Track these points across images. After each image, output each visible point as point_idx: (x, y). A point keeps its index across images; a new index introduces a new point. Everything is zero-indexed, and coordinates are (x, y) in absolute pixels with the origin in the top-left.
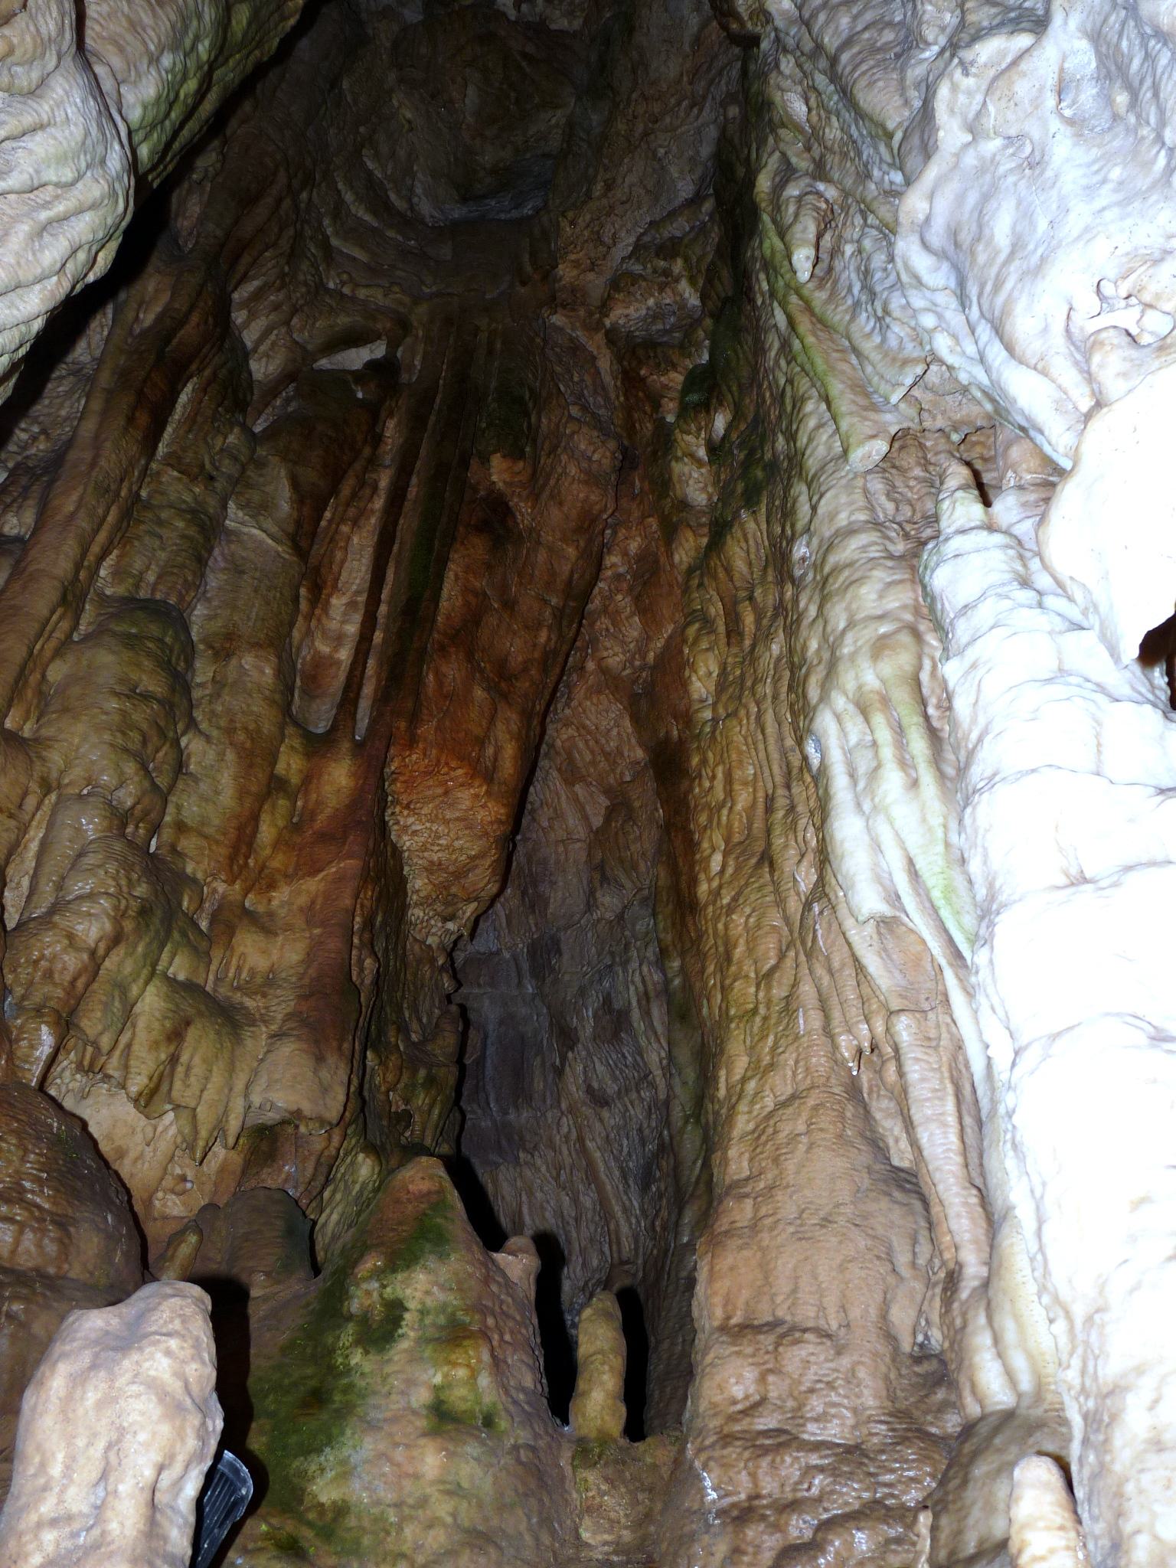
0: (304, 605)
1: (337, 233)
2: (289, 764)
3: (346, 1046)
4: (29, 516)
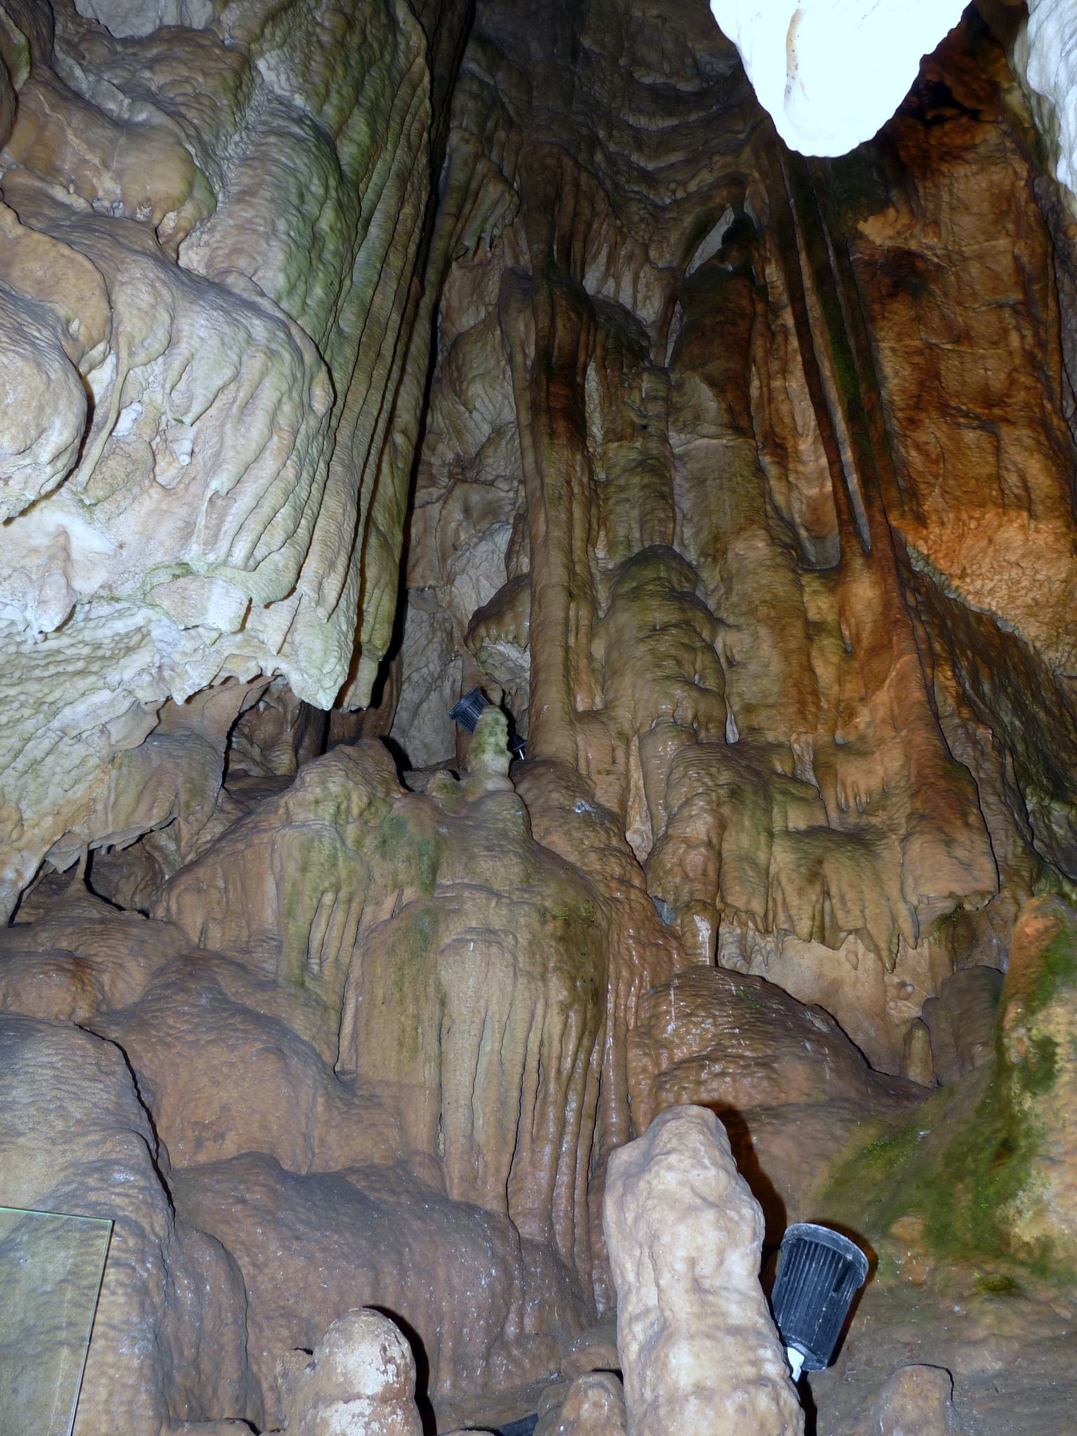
0: (772, 471)
1: (650, 158)
2: (819, 608)
3: (972, 819)
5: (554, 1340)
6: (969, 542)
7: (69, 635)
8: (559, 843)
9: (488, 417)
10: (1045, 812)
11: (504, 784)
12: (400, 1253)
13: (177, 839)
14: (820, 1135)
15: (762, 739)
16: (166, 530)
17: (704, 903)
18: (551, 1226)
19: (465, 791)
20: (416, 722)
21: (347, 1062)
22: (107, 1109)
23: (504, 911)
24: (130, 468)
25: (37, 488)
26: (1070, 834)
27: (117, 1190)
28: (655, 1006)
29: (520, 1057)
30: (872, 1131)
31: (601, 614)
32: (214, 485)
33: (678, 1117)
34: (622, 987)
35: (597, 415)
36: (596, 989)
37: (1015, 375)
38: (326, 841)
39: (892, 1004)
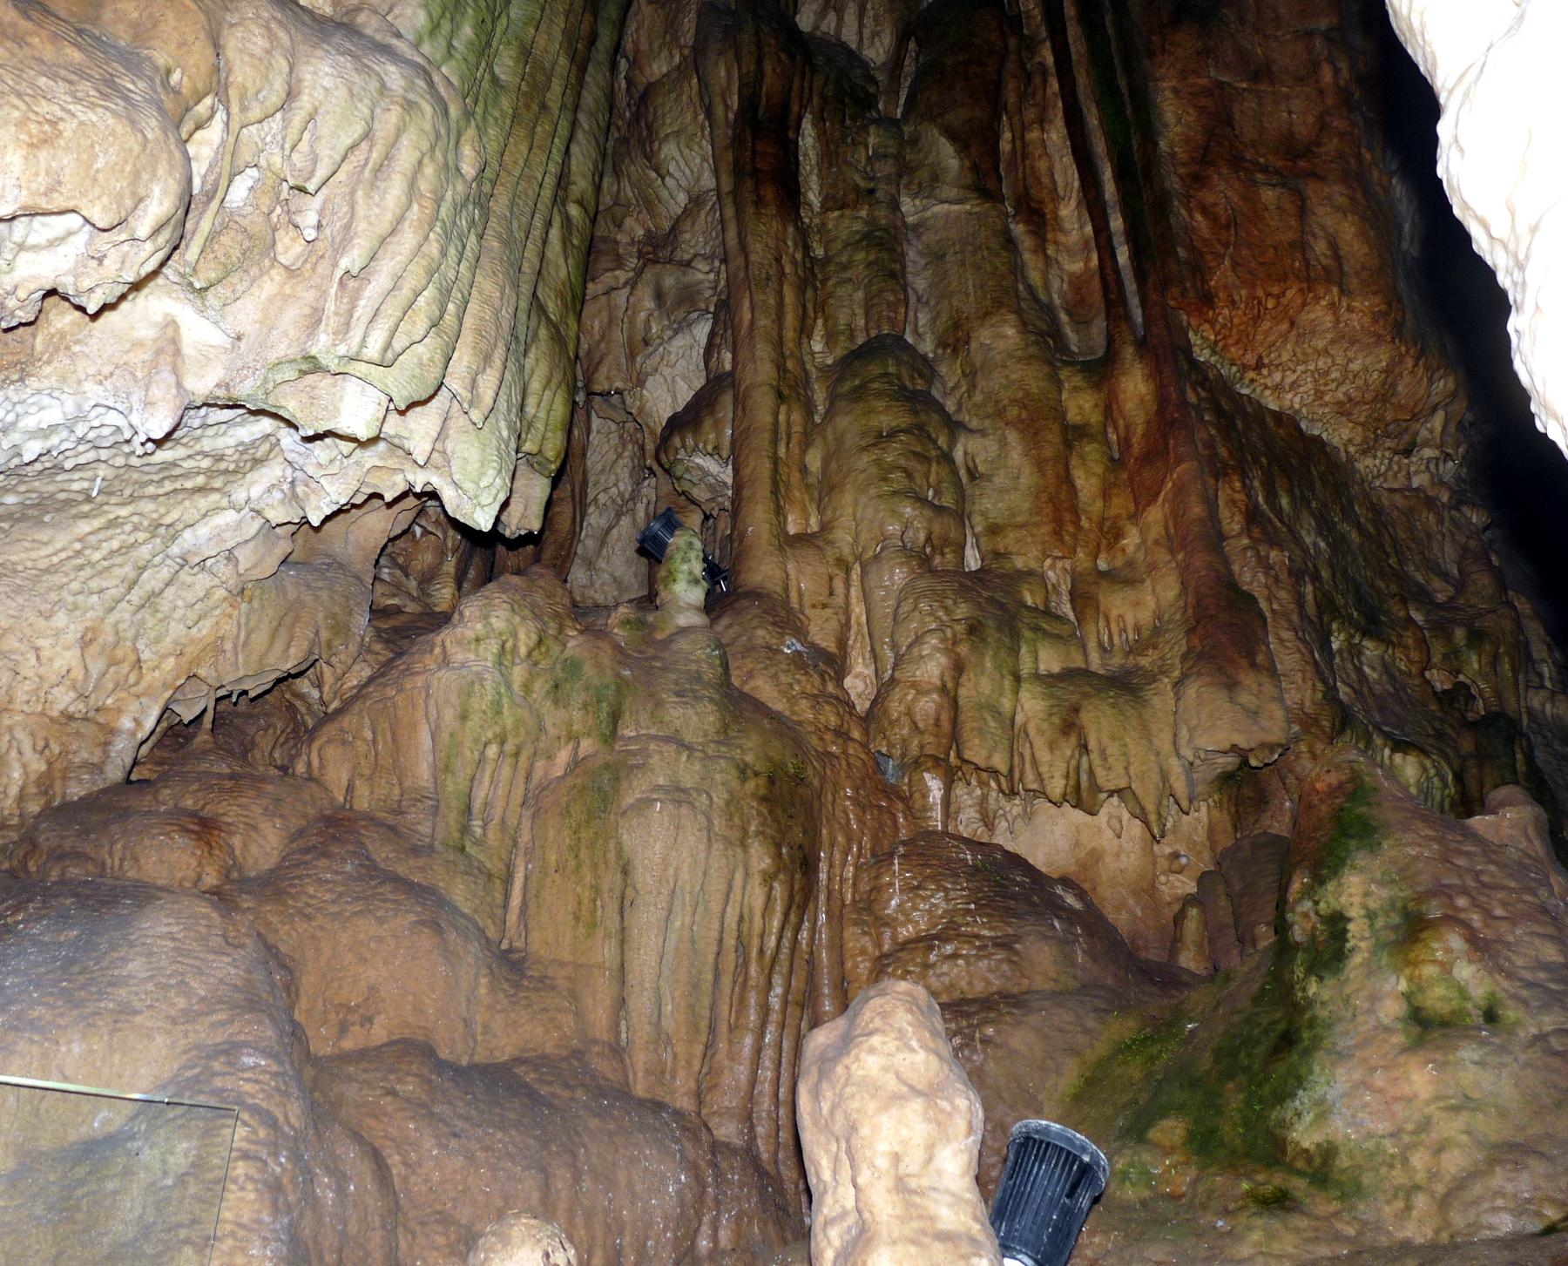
2: (1080, 407)
5: (754, 1256)
6: (1266, 325)
7: (185, 445)
8: (765, 689)
9: (684, 183)
10: (1354, 651)
11: (698, 619)
12: (574, 1155)
13: (319, 685)
14: (1069, 1027)
15: (1008, 566)
16: (292, 316)
17: (936, 759)
18: (752, 1128)
19: (652, 628)
20: (604, 552)
21: (513, 936)
22: (235, 986)
23: (697, 767)
24: (246, 244)
25: (136, 267)
26: (1385, 678)
27: (246, 1075)
28: (876, 878)
29: (715, 935)
30: (1132, 1023)
31: (817, 419)
32: (344, 263)
33: (883, 994)
34: (837, 856)
35: (814, 178)
36: (805, 857)
37: (1328, 119)
38: (489, 685)
39: (1163, 879)
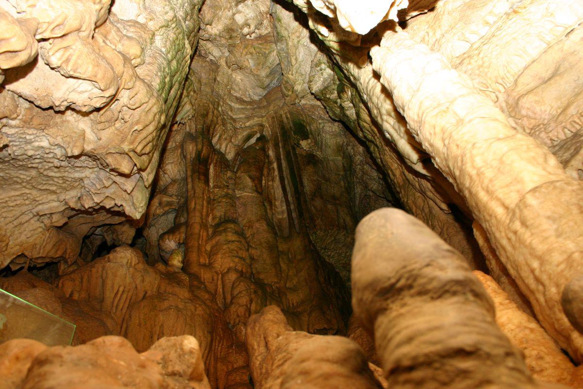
4: (185, 215)
9: (171, 177)
24: (113, 116)
